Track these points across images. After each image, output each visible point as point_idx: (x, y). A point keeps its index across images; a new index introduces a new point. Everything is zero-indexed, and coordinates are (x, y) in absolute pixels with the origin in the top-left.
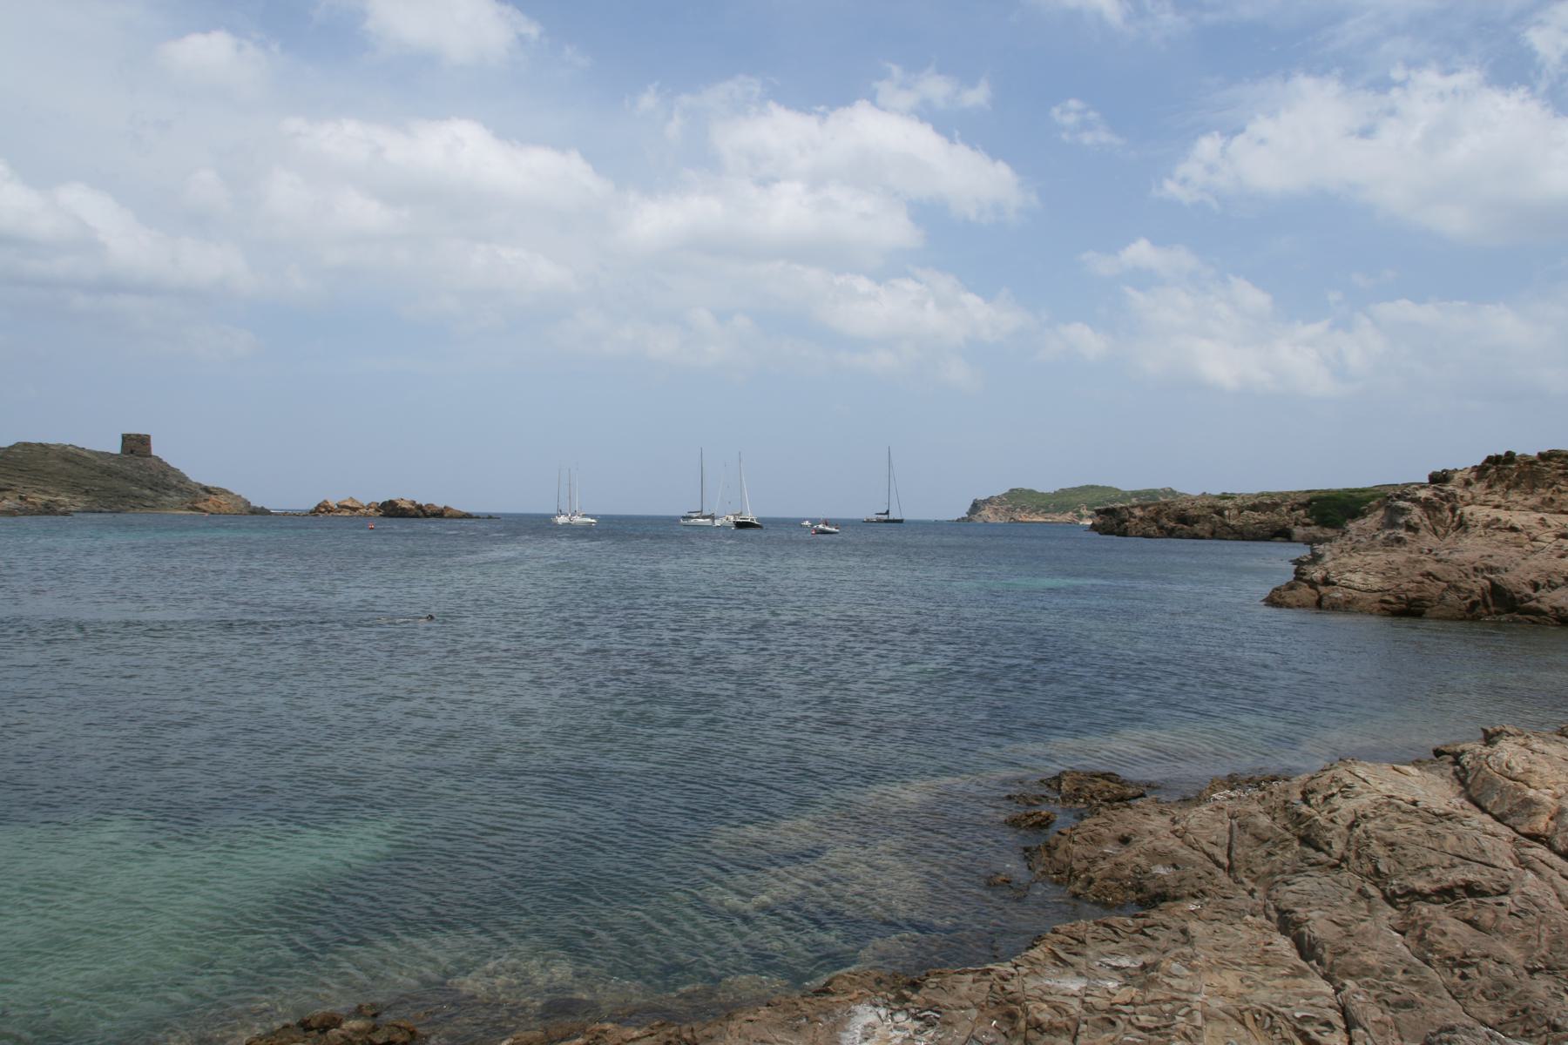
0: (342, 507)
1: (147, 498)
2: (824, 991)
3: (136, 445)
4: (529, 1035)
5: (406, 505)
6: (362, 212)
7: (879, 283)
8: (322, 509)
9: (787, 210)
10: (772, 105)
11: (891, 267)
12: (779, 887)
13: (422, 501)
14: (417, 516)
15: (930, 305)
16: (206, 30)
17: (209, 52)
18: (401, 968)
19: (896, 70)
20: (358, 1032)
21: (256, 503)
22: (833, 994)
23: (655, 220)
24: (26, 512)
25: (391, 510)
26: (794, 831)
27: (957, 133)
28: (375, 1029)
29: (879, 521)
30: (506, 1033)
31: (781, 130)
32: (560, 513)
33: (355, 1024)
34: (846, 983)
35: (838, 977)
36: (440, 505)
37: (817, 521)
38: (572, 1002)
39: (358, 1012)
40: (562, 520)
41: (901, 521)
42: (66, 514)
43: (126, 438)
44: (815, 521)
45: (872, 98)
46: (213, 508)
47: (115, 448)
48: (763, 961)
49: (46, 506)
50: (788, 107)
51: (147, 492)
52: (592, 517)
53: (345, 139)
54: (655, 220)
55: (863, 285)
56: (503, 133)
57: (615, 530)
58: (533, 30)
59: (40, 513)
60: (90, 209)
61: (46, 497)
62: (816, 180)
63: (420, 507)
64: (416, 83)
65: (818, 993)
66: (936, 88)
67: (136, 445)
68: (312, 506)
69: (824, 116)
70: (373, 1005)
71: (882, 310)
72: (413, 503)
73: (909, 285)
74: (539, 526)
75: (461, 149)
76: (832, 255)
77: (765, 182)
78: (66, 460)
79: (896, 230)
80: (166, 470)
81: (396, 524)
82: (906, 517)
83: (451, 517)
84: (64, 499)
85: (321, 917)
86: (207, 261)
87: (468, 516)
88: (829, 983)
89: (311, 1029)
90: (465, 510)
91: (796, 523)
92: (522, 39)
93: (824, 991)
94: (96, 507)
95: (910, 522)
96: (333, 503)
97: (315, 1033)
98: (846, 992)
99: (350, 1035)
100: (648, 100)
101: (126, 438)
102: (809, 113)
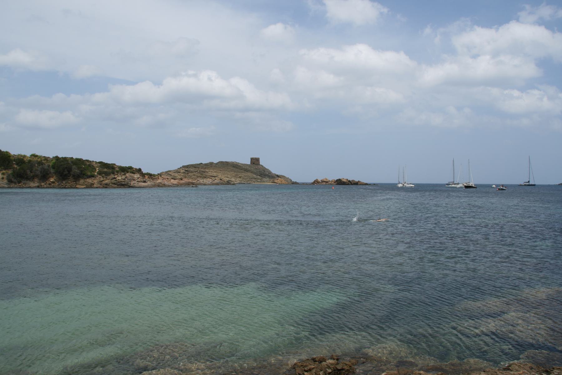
0: (323, 181)
1: (258, 179)
2: (508, 369)
3: (255, 161)
4: (392, 372)
5: (345, 181)
6: (328, 79)
7: (522, 92)
8: (316, 182)
9: (484, 67)
10: (476, 27)
11: (528, 85)
12: (492, 325)
13: (350, 179)
14: (348, 184)
15: (545, 99)
16: (275, 23)
17: (276, 30)
18: (345, 343)
19: (528, 7)
20: (332, 364)
21: (294, 180)
22: (511, 371)
23: (433, 75)
24: (222, 184)
25: (339, 182)
26: (493, 303)
27: (556, 28)
28: (338, 364)
29: (525, 185)
30: (383, 372)
31: (480, 36)
32: (399, 183)
33: (331, 361)
34: (517, 367)
35: (513, 364)
36: (357, 180)
37: (499, 185)
38: (406, 362)
39: (332, 358)
40: (400, 185)
41: (534, 185)
42: (234, 184)
43: (252, 159)
44: (497, 186)
45: (518, 20)
46: (280, 182)
47: (249, 162)
48: (483, 355)
49: (228, 182)
50: (482, 27)
51: (259, 177)
52: (413, 184)
53: (321, 54)
54: (433, 75)
55: (516, 93)
56: (378, 47)
57: (419, 188)
58: (385, 10)
59: (226, 184)
60: (242, 85)
61: (228, 179)
62: (496, 54)
63: (349, 181)
64: (345, 33)
65: (504, 369)
66: (546, 11)
67: (255, 161)
68: (312, 181)
69: (497, 30)
70: (336, 356)
71: (522, 102)
72: (347, 180)
73: (536, 92)
74: (392, 187)
75: (361, 54)
76: (502, 83)
77: (475, 57)
78: (234, 167)
79: (530, 70)
80: (265, 169)
81: (341, 187)
82: (536, 183)
83: (360, 184)
84: (233, 179)
85: (322, 324)
86: (279, 99)
87: (366, 184)
88: (510, 366)
89: (316, 361)
90: (365, 182)
91: (490, 186)
92: (381, 14)
93: (508, 369)
94: (243, 182)
95: (538, 186)
96: (319, 180)
97: (317, 363)
98: (517, 371)
99: (329, 365)
100: (428, 31)
101: (252, 159)
102: (491, 28)
